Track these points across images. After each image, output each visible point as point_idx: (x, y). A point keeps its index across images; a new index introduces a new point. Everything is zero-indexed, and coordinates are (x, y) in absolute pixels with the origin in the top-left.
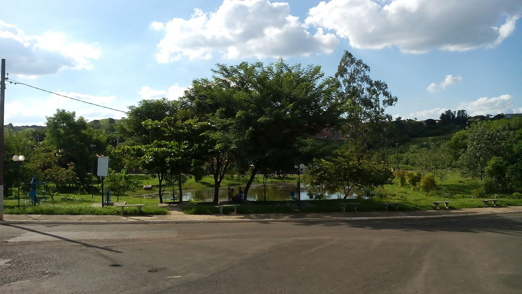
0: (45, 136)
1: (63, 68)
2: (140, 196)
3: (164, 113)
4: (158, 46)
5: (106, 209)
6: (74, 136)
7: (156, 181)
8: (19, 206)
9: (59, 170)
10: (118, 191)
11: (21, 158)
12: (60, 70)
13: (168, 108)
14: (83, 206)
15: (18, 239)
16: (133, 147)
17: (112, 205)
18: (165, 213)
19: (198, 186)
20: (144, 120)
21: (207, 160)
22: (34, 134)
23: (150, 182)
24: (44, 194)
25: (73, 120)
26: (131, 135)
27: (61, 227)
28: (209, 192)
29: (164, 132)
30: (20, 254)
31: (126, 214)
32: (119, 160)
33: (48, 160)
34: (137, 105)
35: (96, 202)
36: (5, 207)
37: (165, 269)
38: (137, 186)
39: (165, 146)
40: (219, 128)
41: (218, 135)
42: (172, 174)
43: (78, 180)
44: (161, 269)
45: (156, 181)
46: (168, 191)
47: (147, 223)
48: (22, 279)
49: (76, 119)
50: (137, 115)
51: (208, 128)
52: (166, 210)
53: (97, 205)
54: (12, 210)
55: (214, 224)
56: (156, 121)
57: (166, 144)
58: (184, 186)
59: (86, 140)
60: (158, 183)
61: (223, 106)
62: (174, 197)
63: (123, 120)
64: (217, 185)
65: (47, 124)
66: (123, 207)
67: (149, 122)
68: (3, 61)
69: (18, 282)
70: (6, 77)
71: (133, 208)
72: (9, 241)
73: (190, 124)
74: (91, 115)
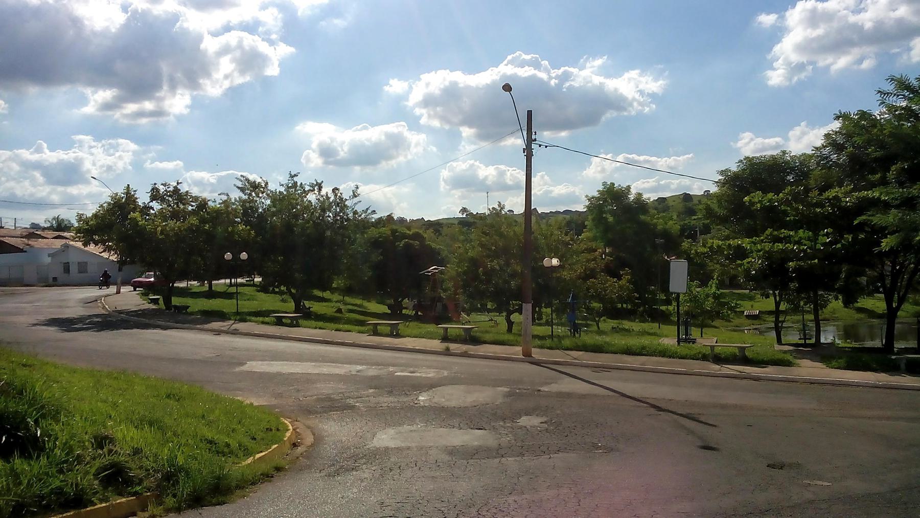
0: (585, 227)
1: (610, 115)
2: (738, 329)
3: (783, 179)
4: (769, 57)
5: (684, 349)
6: (628, 225)
7: (769, 304)
8: (552, 337)
9: (608, 281)
10: (698, 317)
11: (555, 262)
12: (603, 119)
13: (792, 169)
14: (646, 341)
15: (554, 388)
16: (728, 242)
17: (694, 343)
18: (788, 364)
19: (848, 315)
20: (748, 193)
21: (872, 267)
22: (569, 223)
23: (756, 305)
24: (585, 318)
25: (628, 198)
26: (723, 220)
27: (615, 373)
28: (871, 327)
29: (785, 213)
30: (558, 412)
31: (718, 359)
32: (702, 266)
33: (592, 265)
34: (734, 168)
35: (666, 336)
36: (535, 337)
37: (798, 466)
38: (736, 312)
39: (787, 239)
40: (897, 202)
41: (892, 217)
42: (799, 291)
43: (637, 299)
44: (791, 466)
45: (769, 304)
46: (791, 321)
47: (757, 379)
48: (565, 450)
49: (631, 197)
50: (735, 186)
51: (874, 203)
52: (790, 358)
53: (669, 341)
54: (543, 342)
55: (888, 391)
56: (770, 195)
57: (790, 236)
58: (825, 313)
59: (647, 231)
60: (772, 307)
61: (905, 159)
62: (805, 335)
63: (707, 194)
64: (891, 315)
65: (588, 207)
66: (712, 347)
67: (757, 196)
68: (530, 113)
69: (560, 455)
70: (533, 137)
71: (731, 349)
72: (542, 389)
73: (836, 198)
74: (653, 190)
